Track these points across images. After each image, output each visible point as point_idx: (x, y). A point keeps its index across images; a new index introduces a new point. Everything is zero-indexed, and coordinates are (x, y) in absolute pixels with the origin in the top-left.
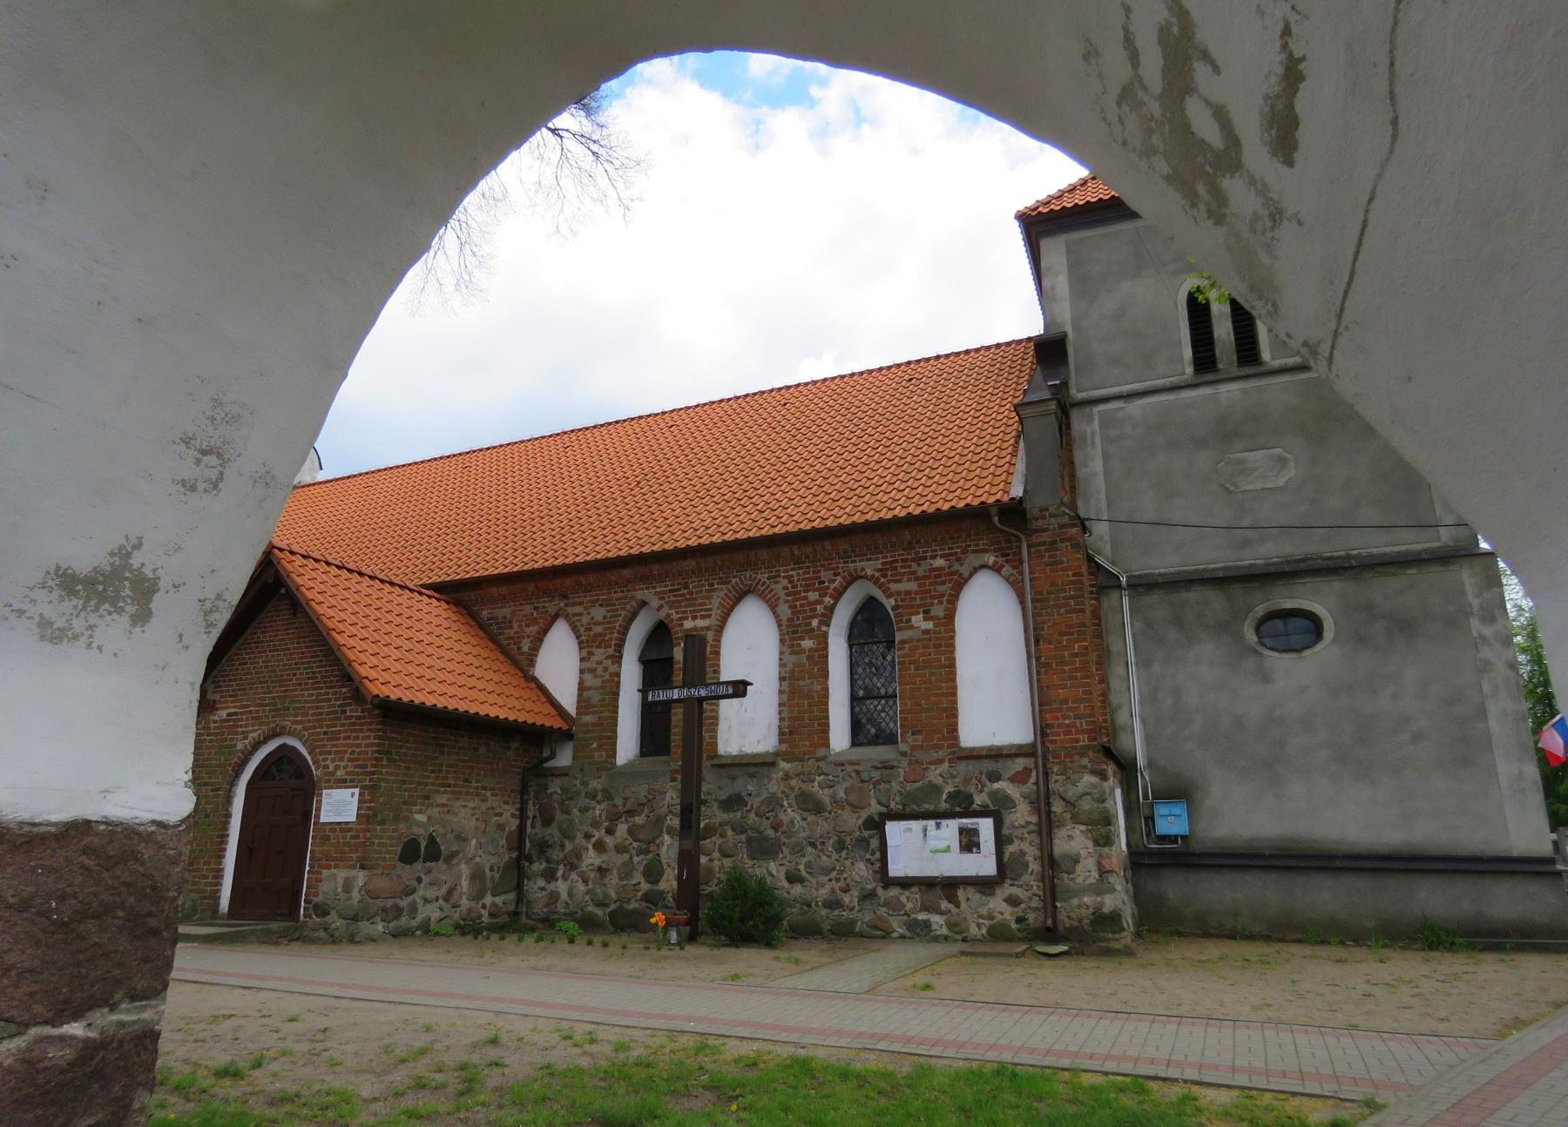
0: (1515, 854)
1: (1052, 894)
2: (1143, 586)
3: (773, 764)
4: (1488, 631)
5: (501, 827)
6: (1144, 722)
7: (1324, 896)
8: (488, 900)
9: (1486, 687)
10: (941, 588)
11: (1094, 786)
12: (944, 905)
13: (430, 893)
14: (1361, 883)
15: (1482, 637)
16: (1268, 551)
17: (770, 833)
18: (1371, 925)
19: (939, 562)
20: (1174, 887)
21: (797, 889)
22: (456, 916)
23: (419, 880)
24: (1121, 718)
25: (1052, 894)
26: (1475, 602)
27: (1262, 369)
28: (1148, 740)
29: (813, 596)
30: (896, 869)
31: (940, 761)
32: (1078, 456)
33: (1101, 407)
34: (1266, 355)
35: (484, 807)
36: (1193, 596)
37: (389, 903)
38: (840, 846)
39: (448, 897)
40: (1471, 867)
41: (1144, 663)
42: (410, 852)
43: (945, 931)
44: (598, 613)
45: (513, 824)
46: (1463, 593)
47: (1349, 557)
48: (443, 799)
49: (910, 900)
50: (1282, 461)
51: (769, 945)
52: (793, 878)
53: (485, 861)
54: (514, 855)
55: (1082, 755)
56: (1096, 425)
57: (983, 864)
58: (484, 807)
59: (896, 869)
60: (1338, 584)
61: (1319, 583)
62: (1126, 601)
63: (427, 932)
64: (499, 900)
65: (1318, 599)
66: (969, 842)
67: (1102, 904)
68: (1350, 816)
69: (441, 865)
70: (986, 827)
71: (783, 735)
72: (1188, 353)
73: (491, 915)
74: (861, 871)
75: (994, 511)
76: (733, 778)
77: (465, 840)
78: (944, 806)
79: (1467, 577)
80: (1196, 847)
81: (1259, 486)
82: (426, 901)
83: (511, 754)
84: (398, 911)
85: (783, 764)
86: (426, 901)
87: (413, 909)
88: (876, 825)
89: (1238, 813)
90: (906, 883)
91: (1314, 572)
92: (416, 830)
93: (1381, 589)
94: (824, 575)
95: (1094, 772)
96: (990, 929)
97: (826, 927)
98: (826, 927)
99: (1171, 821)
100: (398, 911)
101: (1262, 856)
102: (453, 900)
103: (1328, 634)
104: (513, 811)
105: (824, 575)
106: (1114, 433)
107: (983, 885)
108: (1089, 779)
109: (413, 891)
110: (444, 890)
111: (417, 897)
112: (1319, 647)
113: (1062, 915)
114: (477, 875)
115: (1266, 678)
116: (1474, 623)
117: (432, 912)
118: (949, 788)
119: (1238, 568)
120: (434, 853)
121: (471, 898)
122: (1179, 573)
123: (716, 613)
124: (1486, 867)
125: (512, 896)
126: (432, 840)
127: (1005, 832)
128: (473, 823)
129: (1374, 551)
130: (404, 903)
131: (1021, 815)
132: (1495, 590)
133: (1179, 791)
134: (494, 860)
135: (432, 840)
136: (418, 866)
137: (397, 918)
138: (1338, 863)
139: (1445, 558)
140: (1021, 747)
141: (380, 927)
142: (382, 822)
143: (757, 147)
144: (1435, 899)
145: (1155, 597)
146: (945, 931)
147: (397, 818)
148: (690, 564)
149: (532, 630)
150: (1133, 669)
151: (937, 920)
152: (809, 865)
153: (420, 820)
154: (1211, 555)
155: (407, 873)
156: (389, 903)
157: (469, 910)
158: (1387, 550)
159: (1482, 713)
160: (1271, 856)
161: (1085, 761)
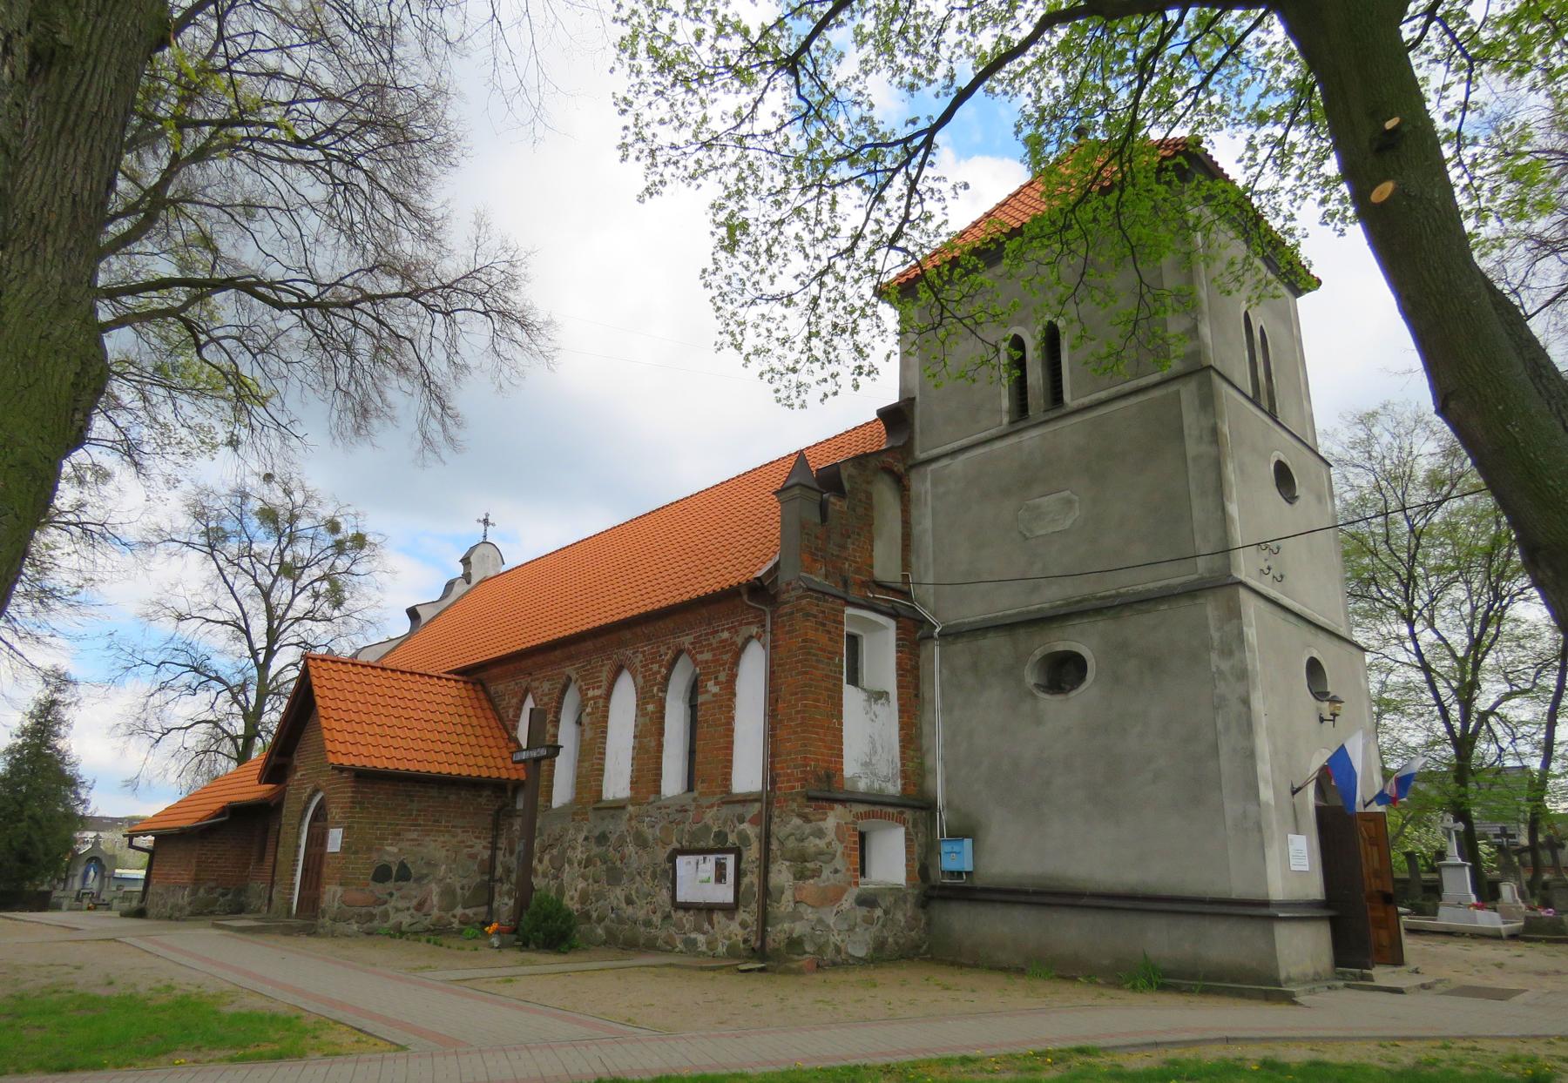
0: (1233, 896)
1: (764, 919)
2: (953, 634)
3: (624, 808)
4: (1225, 666)
5: (472, 857)
6: (945, 764)
7: (1072, 933)
8: (459, 911)
9: (1220, 724)
10: (725, 657)
11: (798, 827)
12: (706, 926)
13: (401, 905)
14: (1102, 921)
15: (1220, 672)
16: (1050, 596)
17: (618, 863)
18: (1106, 962)
19: (726, 635)
20: (960, 920)
21: (630, 910)
22: (835, 938)
23: (391, 895)
24: (928, 763)
25: (764, 919)
26: (1216, 635)
27: (1064, 411)
28: (948, 781)
29: (655, 667)
30: (682, 896)
31: (712, 806)
32: (914, 513)
33: (934, 466)
34: (1067, 397)
35: (454, 841)
36: (989, 642)
37: (364, 910)
38: (654, 876)
39: (419, 907)
40: (1127, 904)
41: (948, 709)
42: (382, 874)
43: (704, 948)
44: (546, 686)
45: (486, 854)
46: (1207, 627)
47: (1118, 595)
48: (414, 835)
49: (687, 919)
50: (1069, 502)
51: (560, 952)
52: (629, 901)
53: (456, 882)
54: (486, 878)
55: (794, 800)
56: (928, 484)
57: (725, 894)
58: (454, 841)
59: (682, 896)
60: (1101, 625)
61: (1083, 624)
62: (937, 650)
63: (399, 933)
64: (470, 912)
65: (1080, 640)
66: (720, 877)
67: (792, 930)
68: (1093, 856)
69: (411, 884)
70: (730, 860)
71: (634, 783)
72: (1005, 403)
73: (461, 922)
74: (665, 895)
75: (743, 590)
76: (603, 819)
77: (436, 865)
78: (711, 843)
79: (1210, 609)
80: (978, 883)
81: (1050, 530)
82: (397, 910)
83: (483, 801)
84: (372, 917)
85: (630, 808)
86: (397, 910)
87: (386, 916)
88: (672, 859)
89: (1011, 854)
90: (687, 907)
91: (1083, 613)
92: (387, 858)
93: (1135, 627)
94: (663, 649)
95: (799, 815)
96: (729, 947)
97: (642, 941)
98: (642, 941)
99: (956, 858)
100: (372, 917)
101: (1026, 893)
102: (425, 910)
103: (1090, 675)
104: (485, 843)
105: (663, 649)
106: (941, 489)
107: (729, 910)
108: (797, 821)
109: (385, 902)
110: (415, 902)
111: (388, 907)
112: (1083, 687)
113: (769, 940)
114: (448, 892)
115: (1038, 720)
116: (1214, 657)
117: (406, 919)
118: (715, 829)
119: (1029, 612)
120: (404, 874)
121: (440, 909)
122: (984, 620)
123: (605, 684)
124: (1206, 908)
125: (484, 909)
126: (403, 866)
127: (743, 866)
128: (444, 853)
129: (1140, 588)
130: (377, 910)
131: (752, 853)
132: (1235, 621)
133: (965, 830)
134: (465, 881)
135: (403, 866)
136: (390, 885)
137: (371, 920)
138: (1084, 901)
139: (1192, 592)
140: (751, 794)
141: (355, 927)
142: (356, 853)
143: (363, 412)
144: (1163, 940)
145: (959, 646)
146: (704, 948)
147: (369, 849)
148: (589, 645)
149: (515, 701)
150: (938, 715)
151: (701, 938)
152: (637, 891)
153: (391, 852)
154: (1008, 603)
155: (379, 889)
156: (364, 910)
157: (440, 918)
158: (1151, 586)
159: (1215, 750)
160: (1035, 893)
161: (795, 806)
